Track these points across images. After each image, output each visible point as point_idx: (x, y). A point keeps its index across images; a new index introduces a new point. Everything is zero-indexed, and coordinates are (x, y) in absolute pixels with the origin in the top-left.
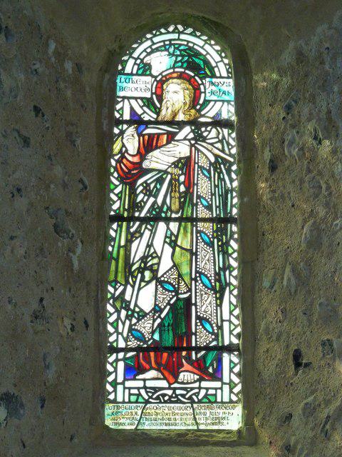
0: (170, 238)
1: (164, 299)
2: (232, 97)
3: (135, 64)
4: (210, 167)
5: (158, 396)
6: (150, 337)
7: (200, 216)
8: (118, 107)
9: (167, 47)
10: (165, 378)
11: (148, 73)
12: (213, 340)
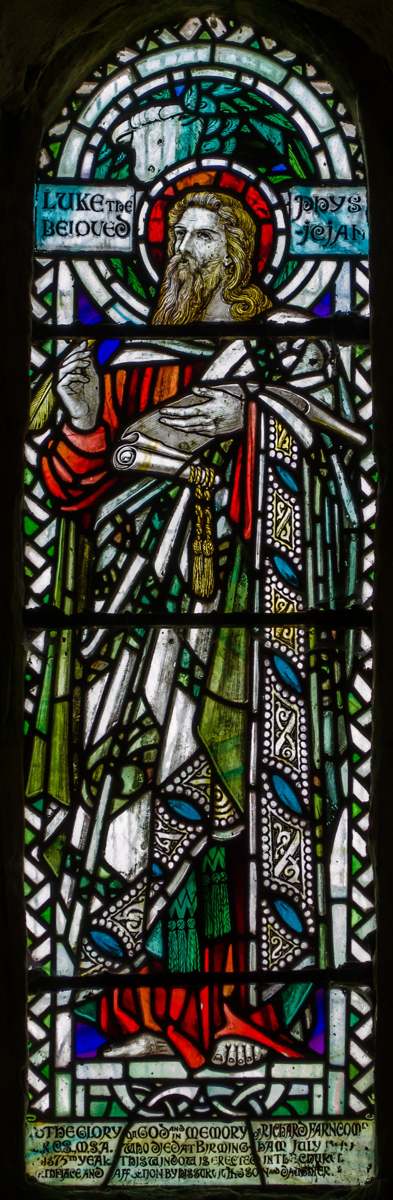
0: (190, 672)
1: (174, 843)
2: (362, 247)
3: (86, 147)
4: (299, 462)
5: (161, 1102)
6: (138, 947)
7: (271, 608)
8: (44, 282)
9: (180, 89)
10: (178, 1056)
11: (124, 173)
12: (305, 954)
